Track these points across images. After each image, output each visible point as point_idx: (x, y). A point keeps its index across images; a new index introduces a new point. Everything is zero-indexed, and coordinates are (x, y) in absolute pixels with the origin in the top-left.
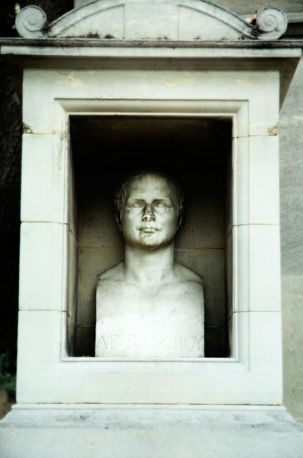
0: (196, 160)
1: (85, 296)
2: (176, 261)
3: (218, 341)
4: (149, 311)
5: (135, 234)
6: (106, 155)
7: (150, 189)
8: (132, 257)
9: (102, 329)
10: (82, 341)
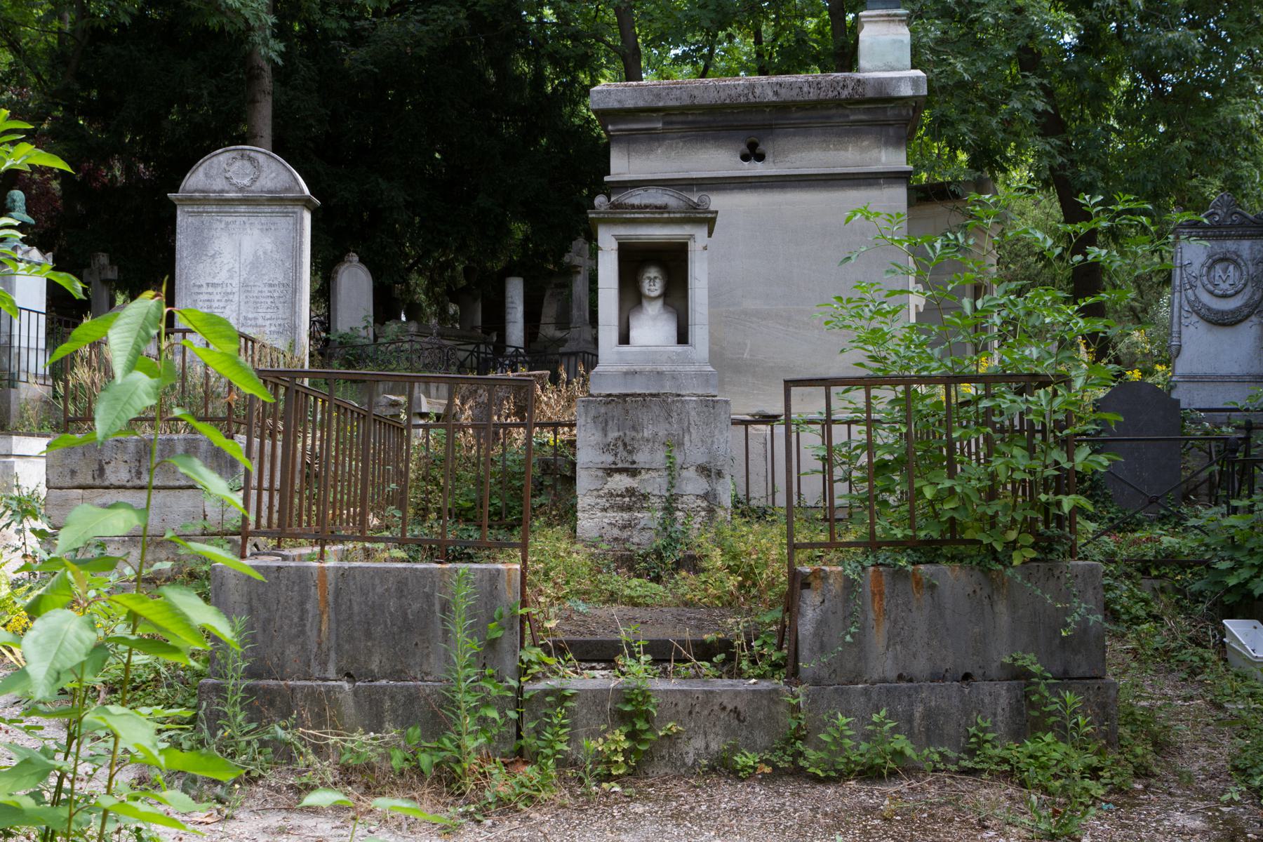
0: (672, 261)
1: (624, 320)
2: (665, 304)
3: (683, 338)
4: (653, 329)
5: (647, 292)
6: (634, 260)
7: (653, 272)
8: (645, 303)
9: (633, 334)
10: (624, 339)
